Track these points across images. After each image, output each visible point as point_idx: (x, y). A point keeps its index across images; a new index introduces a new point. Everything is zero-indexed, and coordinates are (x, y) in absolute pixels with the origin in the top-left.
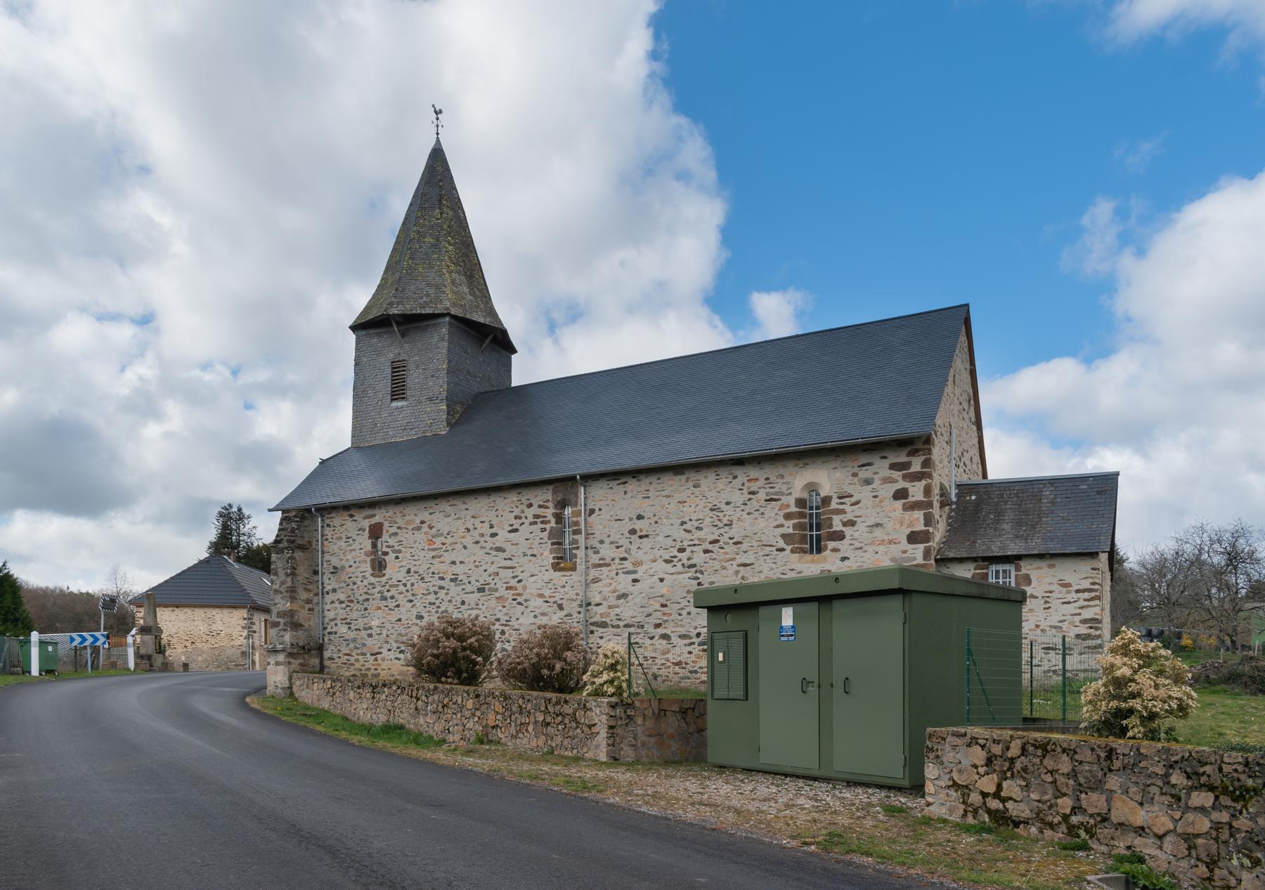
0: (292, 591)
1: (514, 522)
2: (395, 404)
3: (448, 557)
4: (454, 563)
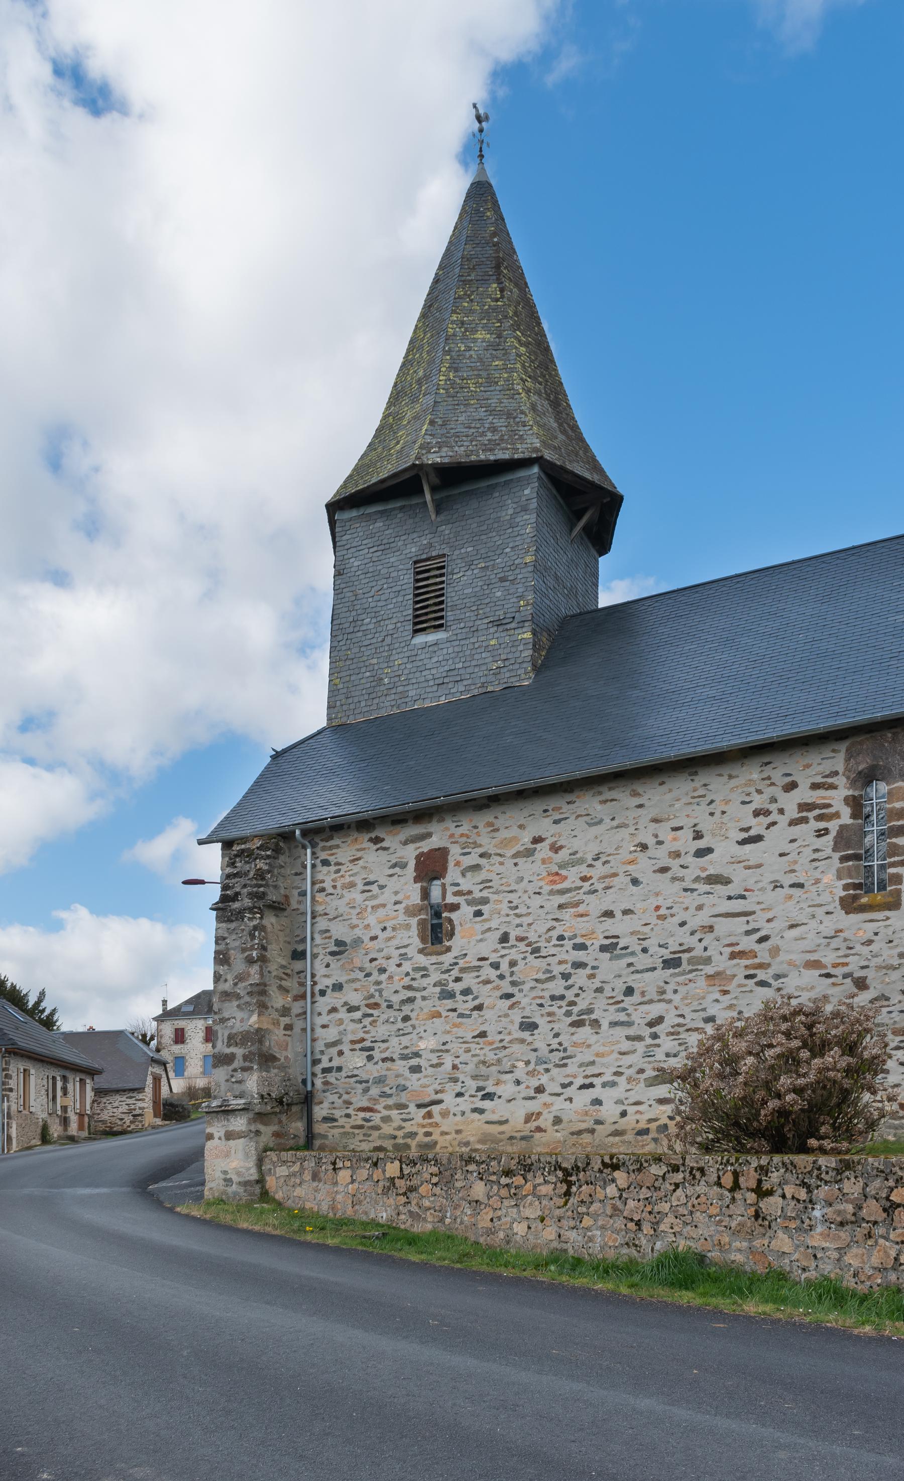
0: (260, 990)
1: (752, 821)
2: (420, 639)
3: (595, 905)
4: (609, 914)
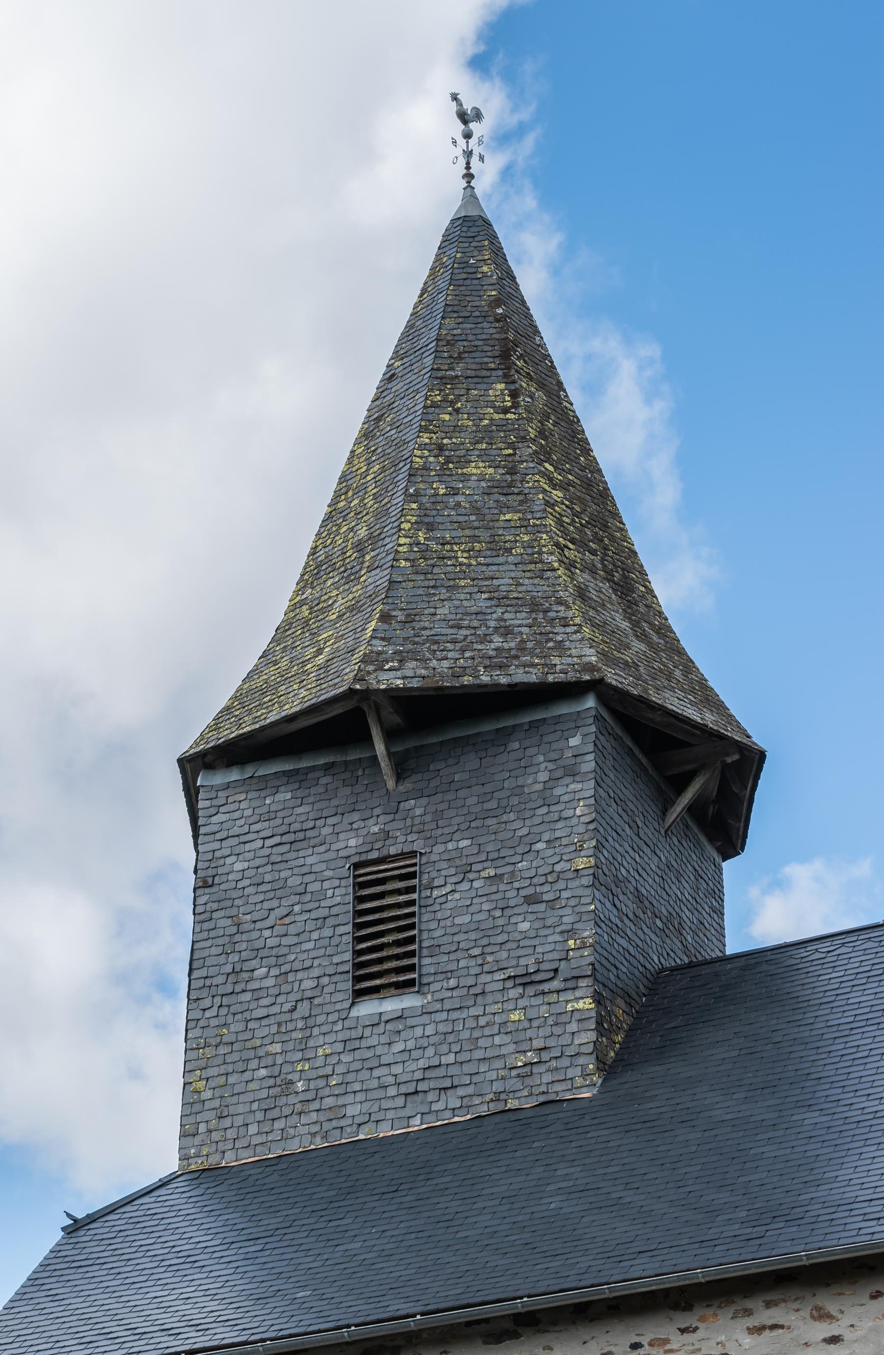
2: (367, 1008)
